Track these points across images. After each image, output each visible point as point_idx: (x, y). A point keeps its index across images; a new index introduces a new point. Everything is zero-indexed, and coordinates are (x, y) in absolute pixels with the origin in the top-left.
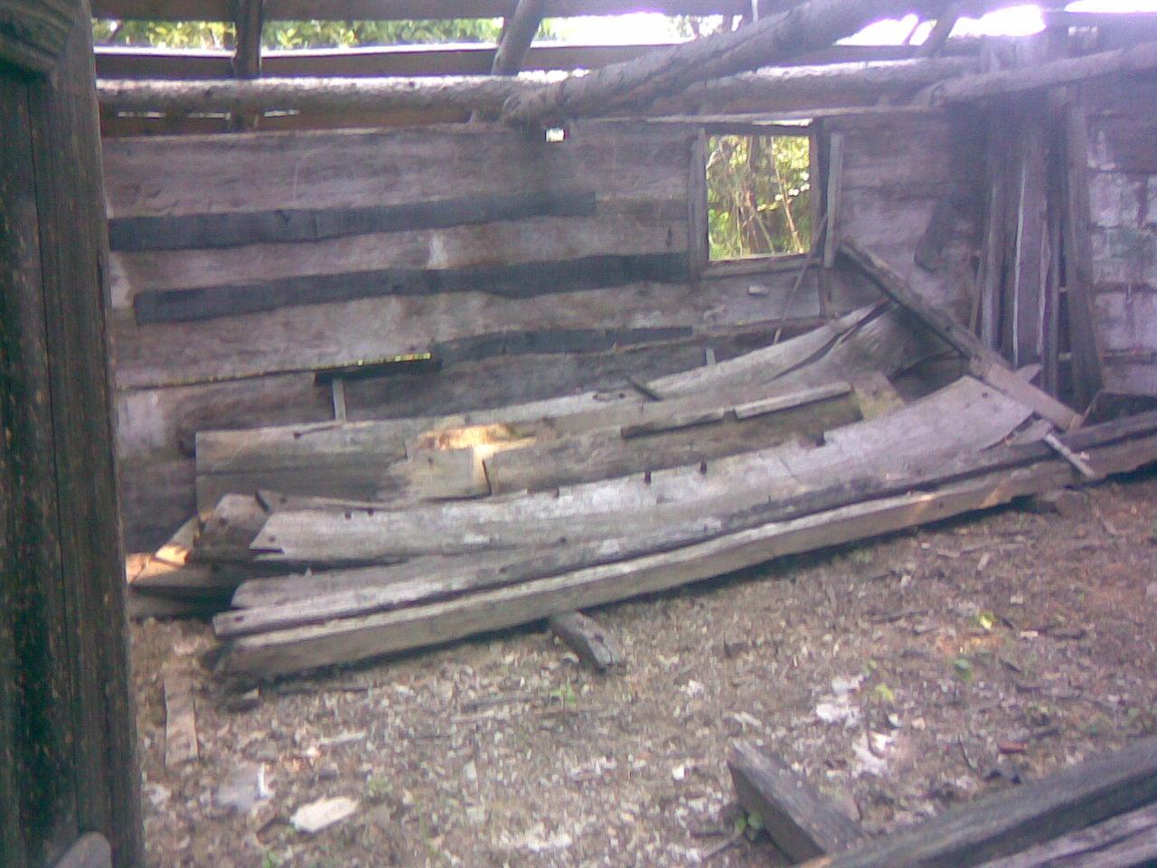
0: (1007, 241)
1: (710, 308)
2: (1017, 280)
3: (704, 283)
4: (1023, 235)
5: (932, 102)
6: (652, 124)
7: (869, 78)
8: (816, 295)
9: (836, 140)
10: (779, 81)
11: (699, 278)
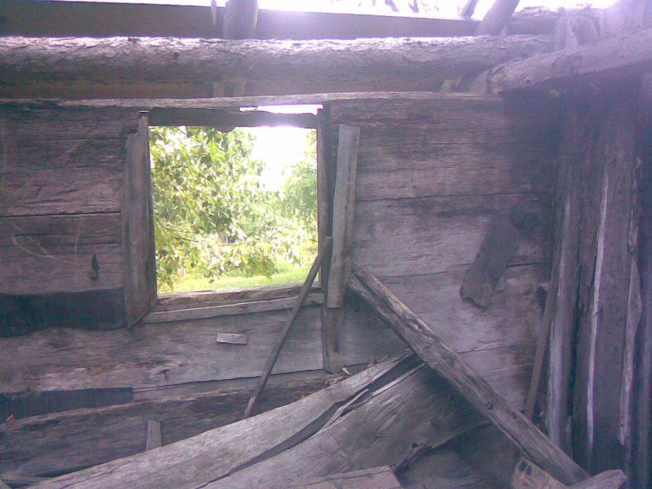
0: (582, 274)
1: (160, 362)
2: (595, 331)
3: (150, 330)
4: (603, 274)
5: (489, 90)
6: (64, 108)
7: (409, 56)
8: (319, 343)
9: (346, 134)
10: (285, 55)
11: (140, 323)
